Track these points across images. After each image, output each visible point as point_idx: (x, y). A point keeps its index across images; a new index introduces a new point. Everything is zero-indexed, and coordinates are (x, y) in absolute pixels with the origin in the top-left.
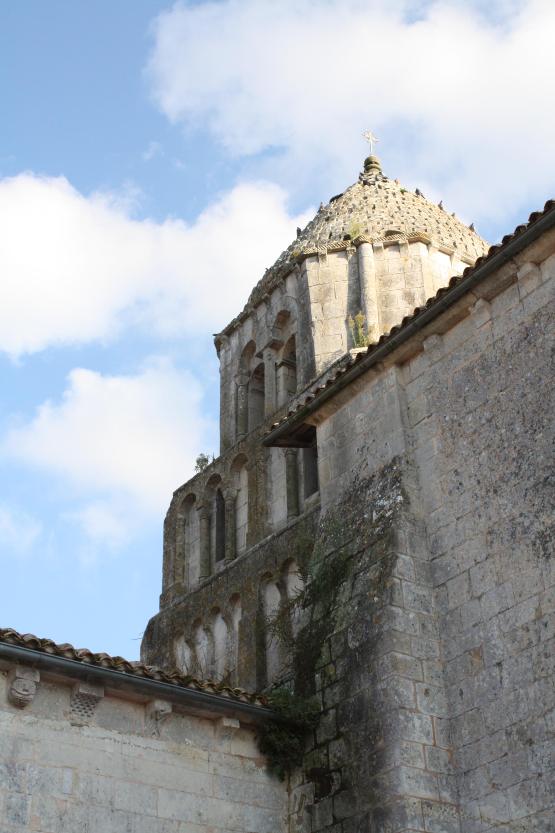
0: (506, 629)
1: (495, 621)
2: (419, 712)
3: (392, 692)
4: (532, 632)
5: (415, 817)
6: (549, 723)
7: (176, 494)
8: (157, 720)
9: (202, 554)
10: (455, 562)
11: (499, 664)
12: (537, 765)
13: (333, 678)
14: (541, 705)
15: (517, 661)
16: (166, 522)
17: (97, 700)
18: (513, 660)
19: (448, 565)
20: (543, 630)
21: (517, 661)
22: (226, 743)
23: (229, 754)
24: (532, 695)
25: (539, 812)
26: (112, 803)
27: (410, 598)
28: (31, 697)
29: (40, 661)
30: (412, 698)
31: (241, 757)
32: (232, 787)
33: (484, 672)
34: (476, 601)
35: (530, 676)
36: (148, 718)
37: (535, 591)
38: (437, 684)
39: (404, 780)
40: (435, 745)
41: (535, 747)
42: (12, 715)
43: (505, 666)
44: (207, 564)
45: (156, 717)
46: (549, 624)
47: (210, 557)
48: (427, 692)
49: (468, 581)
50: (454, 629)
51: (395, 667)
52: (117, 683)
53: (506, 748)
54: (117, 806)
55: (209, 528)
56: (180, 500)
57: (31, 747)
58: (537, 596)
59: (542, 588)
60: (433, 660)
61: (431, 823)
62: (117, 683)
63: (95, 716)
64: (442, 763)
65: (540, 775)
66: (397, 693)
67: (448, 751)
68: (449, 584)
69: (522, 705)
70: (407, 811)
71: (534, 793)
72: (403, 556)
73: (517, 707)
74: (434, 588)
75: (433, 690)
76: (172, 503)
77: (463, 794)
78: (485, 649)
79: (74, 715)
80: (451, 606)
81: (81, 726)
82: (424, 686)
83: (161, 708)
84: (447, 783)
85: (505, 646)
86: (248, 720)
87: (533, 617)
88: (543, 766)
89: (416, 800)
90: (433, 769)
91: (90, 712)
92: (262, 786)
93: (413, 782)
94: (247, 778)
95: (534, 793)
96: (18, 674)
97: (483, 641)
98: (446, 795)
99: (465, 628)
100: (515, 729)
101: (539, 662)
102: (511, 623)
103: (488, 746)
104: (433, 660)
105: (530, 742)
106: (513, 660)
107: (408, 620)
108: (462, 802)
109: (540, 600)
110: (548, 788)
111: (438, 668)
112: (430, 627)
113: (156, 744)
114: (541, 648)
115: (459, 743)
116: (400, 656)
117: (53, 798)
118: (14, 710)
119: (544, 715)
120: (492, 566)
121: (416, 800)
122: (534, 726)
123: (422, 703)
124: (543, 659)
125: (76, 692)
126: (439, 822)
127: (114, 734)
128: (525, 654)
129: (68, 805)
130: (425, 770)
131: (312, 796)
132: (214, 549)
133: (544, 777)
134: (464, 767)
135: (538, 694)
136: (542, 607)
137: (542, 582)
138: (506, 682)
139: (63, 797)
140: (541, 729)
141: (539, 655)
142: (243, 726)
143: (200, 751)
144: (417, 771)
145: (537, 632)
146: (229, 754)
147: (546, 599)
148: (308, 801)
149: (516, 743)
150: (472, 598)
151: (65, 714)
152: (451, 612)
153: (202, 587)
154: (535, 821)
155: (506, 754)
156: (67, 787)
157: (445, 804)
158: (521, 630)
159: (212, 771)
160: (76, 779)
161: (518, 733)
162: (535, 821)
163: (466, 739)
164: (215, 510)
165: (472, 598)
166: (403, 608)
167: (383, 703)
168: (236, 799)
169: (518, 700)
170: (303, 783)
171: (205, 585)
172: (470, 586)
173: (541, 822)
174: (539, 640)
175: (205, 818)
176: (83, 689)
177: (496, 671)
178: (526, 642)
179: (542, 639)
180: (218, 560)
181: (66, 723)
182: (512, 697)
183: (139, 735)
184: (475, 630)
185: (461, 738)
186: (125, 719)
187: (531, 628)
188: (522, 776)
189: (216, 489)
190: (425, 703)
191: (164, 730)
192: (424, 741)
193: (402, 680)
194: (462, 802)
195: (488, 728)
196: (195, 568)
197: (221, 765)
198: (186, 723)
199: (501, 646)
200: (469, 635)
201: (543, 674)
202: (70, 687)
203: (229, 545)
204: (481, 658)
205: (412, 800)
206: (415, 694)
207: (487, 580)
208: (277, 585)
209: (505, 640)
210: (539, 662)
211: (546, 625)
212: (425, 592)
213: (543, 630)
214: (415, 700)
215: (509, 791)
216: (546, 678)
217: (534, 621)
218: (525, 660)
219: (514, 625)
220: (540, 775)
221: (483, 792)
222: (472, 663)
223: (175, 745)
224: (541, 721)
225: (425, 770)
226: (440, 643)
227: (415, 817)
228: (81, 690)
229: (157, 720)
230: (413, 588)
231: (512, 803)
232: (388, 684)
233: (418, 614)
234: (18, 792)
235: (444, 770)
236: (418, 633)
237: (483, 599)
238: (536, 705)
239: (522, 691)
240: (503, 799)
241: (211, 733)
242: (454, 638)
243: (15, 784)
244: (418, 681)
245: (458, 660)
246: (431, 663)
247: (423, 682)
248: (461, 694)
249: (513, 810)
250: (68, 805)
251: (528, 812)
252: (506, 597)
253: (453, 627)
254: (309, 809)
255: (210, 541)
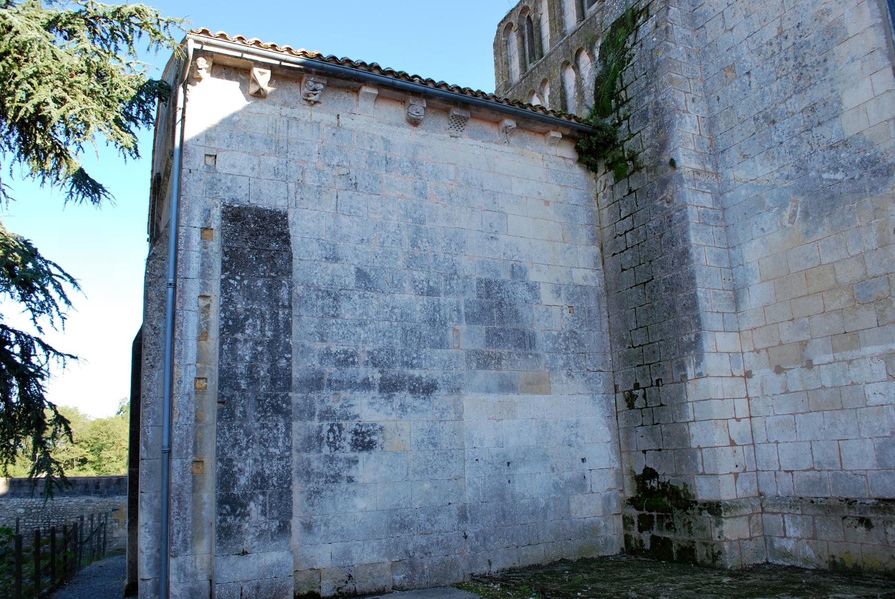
0: (753, 47)
1: (744, 43)
2: (689, 113)
3: (670, 100)
4: (774, 45)
5: (689, 180)
6: (789, 106)
7: (499, 25)
8: (507, 133)
9: (520, 59)
10: (712, 8)
11: (748, 73)
12: (779, 136)
13: (625, 100)
14: (782, 95)
15: (762, 68)
16: (494, 44)
17: (466, 119)
18: (759, 68)
19: (706, 12)
20: (784, 42)
21: (762, 68)
22: (553, 148)
23: (556, 155)
24: (774, 89)
25: (779, 168)
26: (482, 186)
27: (679, 36)
28: (422, 117)
29: (425, 92)
30: (684, 103)
31: (564, 158)
32: (559, 176)
33: (736, 81)
34: (730, 33)
35: (773, 76)
36: (501, 132)
37: (777, 15)
38: (700, 95)
39: (681, 156)
40: (700, 135)
41: (777, 125)
42: (410, 131)
43: (752, 73)
44: (523, 66)
45: (507, 131)
46: (789, 37)
47: (525, 61)
48: (693, 101)
49: (722, 20)
50: (712, 56)
51: (671, 82)
52: (479, 106)
53: (754, 130)
54: (485, 188)
55: (523, 43)
56: (502, 29)
57: (426, 151)
58: (779, 19)
59: (783, 12)
60: (697, 79)
61: (700, 184)
62: (479, 106)
63: (465, 132)
64: (706, 147)
65: (781, 143)
66: (674, 100)
67: (709, 138)
68: (706, 25)
69: (767, 98)
70: (684, 176)
71: (776, 156)
72: (673, 8)
73: (763, 100)
74: (695, 30)
75: (697, 99)
76: (498, 32)
77: (720, 166)
78: (736, 65)
79: (451, 130)
80: (709, 40)
81: (457, 137)
82: (692, 96)
83: (509, 124)
84: (709, 159)
85: (752, 59)
86: (567, 132)
87: (776, 34)
88: (784, 137)
89: (689, 170)
90: (699, 150)
91: (462, 128)
92: (579, 176)
93: (687, 158)
94: (568, 171)
95: (776, 156)
96: (411, 102)
97: (735, 59)
98: (709, 167)
99: (720, 54)
100: (761, 115)
101: (781, 65)
102: (757, 42)
103: (739, 131)
104: (697, 79)
105: (774, 122)
106: (759, 68)
107: (679, 52)
108: (719, 171)
109: (781, 21)
110: (787, 151)
111: (701, 84)
112: (693, 57)
113: (506, 148)
114: (782, 55)
115: (717, 133)
116: (674, 75)
117: (443, 182)
118: (411, 127)
119: (785, 101)
120: (742, 5)
121: (689, 170)
122: (776, 111)
123: (691, 106)
124: (784, 62)
125: (451, 115)
126: (705, 184)
127: (479, 142)
128: (769, 62)
129: (454, 187)
130: (695, 151)
131: (613, 179)
132: (527, 56)
133: (784, 144)
134: (721, 148)
135: (780, 88)
136: (783, 25)
137: (783, 7)
138: (754, 85)
139: (450, 182)
140: (782, 112)
141: (781, 60)
142: (564, 137)
143: (537, 154)
144: (689, 151)
145: (779, 44)
146: (556, 155)
147: (786, 19)
148: (610, 183)
149: (761, 124)
150: (726, 31)
151: (446, 129)
152: (709, 45)
153: (522, 80)
154: (777, 175)
155: (754, 134)
156: (452, 176)
157: (708, 172)
158: (765, 46)
159: (545, 167)
160: (457, 171)
161: (763, 117)
162: (777, 175)
163: (723, 129)
164: (526, 31)
165: (726, 31)
166: (675, 43)
167: (663, 108)
168: (563, 184)
169: (763, 96)
170: (606, 172)
171: (524, 78)
172: (724, 22)
173: (782, 175)
174: (780, 50)
175: (543, 195)
176: (456, 112)
177: (746, 77)
178: (770, 53)
179: (783, 48)
180: (530, 62)
181: (447, 136)
182: (758, 94)
183: (495, 143)
184: (728, 53)
185: (719, 129)
186: (485, 133)
187: (774, 43)
188: (767, 146)
189: (526, 17)
190: (693, 107)
191: (512, 140)
192: (693, 131)
193: (676, 91)
194: (719, 171)
195: (739, 118)
196: (516, 70)
197: (551, 163)
198: (526, 135)
199: (749, 60)
200: (724, 58)
201: (785, 73)
202: (447, 111)
203: (537, 50)
204: (734, 71)
205: (687, 170)
206: (686, 101)
207: (737, 15)
208: (573, 67)
209: (752, 55)
210: (781, 65)
211: (786, 38)
212: (689, 33)
213: (784, 42)
214: (686, 105)
215: (756, 158)
216: (786, 75)
217: (777, 37)
218: (769, 66)
219: (760, 43)
220: (781, 143)
221: (736, 162)
222: (726, 77)
223: (520, 150)
224: (782, 106)
225: (695, 151)
226: (701, 68)
227: (689, 180)
228: (455, 113)
229: (507, 133)
230: (681, 29)
231: (759, 165)
232: (667, 95)
233: (685, 48)
234: (420, 179)
235: (707, 151)
236: (685, 60)
237: (734, 30)
238: (778, 95)
239: (767, 89)
240: (751, 164)
241: (543, 143)
242: (712, 62)
243: (417, 174)
244: (687, 93)
245: (715, 76)
246: (695, 81)
247: (691, 93)
248: (718, 99)
249: (759, 170)
250: (454, 187)
251: (771, 169)
252: (753, 24)
253: (711, 54)
254: (612, 187)
255: (524, 51)
